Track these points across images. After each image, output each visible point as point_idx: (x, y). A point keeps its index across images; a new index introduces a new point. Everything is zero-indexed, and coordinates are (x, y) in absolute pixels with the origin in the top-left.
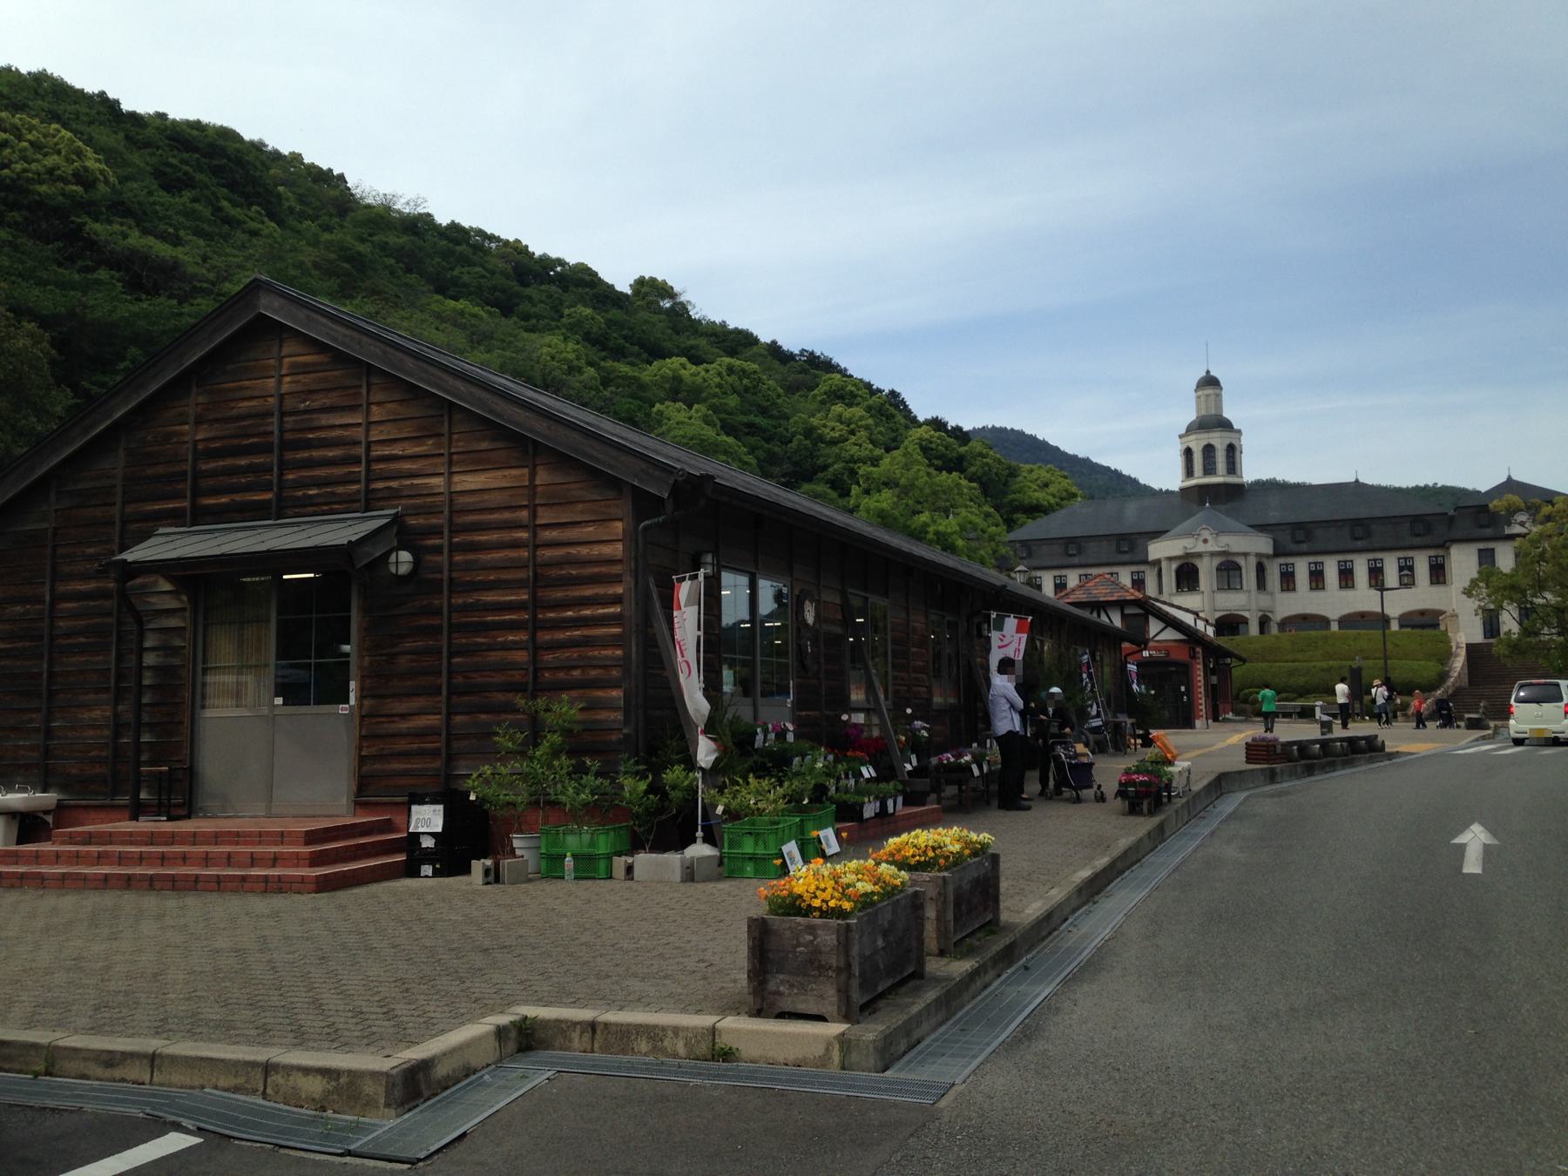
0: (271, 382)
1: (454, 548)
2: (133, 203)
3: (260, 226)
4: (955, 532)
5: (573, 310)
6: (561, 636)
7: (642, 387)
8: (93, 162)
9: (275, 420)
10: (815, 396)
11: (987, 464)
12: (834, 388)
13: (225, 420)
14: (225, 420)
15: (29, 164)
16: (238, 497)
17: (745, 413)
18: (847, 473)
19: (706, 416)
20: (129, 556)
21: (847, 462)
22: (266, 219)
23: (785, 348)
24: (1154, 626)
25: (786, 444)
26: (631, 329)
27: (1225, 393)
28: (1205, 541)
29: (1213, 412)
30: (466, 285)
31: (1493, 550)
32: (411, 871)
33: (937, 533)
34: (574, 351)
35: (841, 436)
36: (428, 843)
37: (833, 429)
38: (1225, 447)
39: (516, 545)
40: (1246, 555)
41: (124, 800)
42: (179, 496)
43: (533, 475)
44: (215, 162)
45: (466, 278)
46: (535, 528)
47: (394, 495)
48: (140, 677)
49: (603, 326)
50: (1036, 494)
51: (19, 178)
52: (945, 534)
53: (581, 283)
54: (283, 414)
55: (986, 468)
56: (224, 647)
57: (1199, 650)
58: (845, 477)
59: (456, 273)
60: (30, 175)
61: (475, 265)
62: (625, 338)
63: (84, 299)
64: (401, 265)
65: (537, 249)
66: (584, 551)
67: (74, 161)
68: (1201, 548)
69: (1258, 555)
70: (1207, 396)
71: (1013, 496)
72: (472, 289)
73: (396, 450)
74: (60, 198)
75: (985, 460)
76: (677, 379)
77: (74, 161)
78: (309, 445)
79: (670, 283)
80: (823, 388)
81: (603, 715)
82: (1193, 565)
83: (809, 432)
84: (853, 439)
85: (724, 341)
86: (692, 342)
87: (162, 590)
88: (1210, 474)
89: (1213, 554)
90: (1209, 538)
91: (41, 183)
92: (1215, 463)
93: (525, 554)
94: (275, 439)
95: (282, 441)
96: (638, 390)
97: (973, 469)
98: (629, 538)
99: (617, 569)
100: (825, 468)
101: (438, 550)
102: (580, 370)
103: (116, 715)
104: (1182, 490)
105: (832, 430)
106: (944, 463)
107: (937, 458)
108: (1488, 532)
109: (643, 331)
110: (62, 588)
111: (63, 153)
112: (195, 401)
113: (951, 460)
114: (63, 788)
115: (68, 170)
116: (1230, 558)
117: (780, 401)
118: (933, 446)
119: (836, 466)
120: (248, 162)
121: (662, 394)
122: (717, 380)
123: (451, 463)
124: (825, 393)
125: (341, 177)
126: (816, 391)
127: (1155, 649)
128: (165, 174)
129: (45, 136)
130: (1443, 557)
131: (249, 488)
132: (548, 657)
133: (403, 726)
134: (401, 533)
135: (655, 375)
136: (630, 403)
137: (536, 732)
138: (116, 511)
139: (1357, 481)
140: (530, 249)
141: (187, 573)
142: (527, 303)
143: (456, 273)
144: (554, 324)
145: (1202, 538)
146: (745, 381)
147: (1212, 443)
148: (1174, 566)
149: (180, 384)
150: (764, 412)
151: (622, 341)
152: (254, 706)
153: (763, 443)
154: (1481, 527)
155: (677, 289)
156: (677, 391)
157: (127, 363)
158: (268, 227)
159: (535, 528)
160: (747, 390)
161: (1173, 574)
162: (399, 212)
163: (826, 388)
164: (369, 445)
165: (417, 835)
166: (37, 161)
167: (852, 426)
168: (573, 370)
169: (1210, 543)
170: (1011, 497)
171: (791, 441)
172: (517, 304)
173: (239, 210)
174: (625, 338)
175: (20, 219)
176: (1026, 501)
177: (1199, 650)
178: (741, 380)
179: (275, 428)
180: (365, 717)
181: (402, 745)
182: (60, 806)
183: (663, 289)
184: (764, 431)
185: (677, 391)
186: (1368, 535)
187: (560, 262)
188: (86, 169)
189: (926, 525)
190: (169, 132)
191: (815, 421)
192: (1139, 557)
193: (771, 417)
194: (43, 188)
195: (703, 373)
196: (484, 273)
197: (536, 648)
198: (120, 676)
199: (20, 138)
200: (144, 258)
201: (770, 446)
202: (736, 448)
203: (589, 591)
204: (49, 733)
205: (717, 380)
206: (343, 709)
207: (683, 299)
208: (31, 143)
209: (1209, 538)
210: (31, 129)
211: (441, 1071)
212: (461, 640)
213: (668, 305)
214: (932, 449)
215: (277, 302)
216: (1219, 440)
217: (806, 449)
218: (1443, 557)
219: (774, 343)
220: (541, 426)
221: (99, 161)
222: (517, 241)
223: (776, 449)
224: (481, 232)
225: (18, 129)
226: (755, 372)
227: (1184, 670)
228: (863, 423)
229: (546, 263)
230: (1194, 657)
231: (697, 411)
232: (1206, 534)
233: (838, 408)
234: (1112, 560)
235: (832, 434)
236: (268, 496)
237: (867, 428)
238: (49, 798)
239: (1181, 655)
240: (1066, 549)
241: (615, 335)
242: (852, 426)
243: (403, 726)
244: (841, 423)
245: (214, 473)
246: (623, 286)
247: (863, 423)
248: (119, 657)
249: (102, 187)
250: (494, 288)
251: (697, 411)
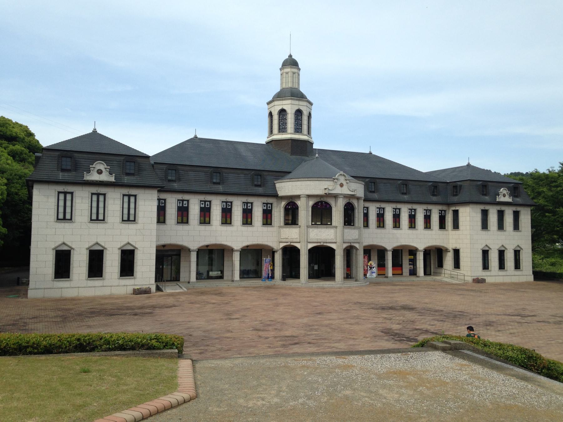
27: (301, 73)
28: (342, 185)
29: (290, 85)
38: (294, 111)
68: (338, 190)
69: (309, 196)
70: (287, 73)
88: (283, 132)
90: (344, 183)
104: (268, 143)
130: (445, 211)
139: (371, 153)
147: (284, 108)
148: (311, 203)
152: (268, 278)
161: (310, 209)
169: (345, 187)
176: (8, 133)
192: (270, 192)
209: (344, 183)
216: (290, 106)
218: (445, 211)
232: (342, 180)
234: (249, 191)
240: (212, 178)
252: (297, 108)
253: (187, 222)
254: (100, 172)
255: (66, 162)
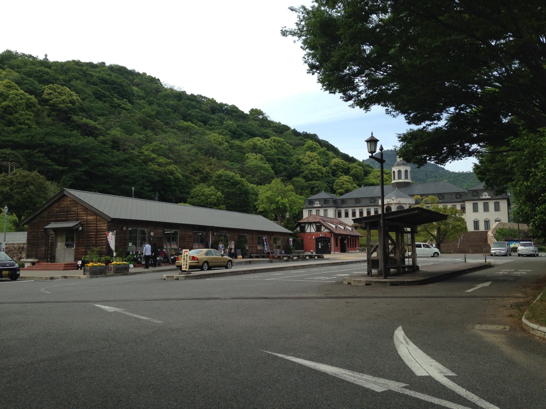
0: (66, 203)
1: (87, 227)
2: (85, 107)
3: (126, 106)
4: (287, 202)
5: (226, 122)
6: (99, 239)
7: (243, 148)
8: (75, 97)
9: (66, 208)
10: (303, 148)
11: (357, 170)
12: (309, 146)
13: (61, 208)
14: (61, 208)
15: (57, 99)
16: (62, 219)
17: (278, 155)
18: (309, 174)
19: (262, 157)
20: (46, 227)
21: (310, 170)
22: (128, 103)
23: (298, 131)
24: (323, 228)
25: (291, 164)
26: (245, 128)
28: (393, 200)
30: (193, 116)
31: (477, 203)
32: (78, 269)
33: (281, 203)
34: (222, 138)
35: (308, 162)
36: (80, 266)
37: (306, 160)
38: (404, 171)
39: (94, 226)
40: (406, 204)
41: (46, 261)
42: (53, 218)
43: (97, 217)
44: (114, 86)
45: (193, 113)
46: (97, 224)
47: (80, 219)
48: (48, 243)
49: (236, 127)
50: (373, 180)
51: (55, 103)
52: (284, 203)
53: (233, 111)
54: (67, 207)
55: (356, 172)
56: (59, 239)
57: (333, 234)
58: (309, 175)
59: (190, 112)
60: (58, 102)
61: (197, 108)
62: (243, 131)
63: (69, 140)
64: (173, 110)
65: (219, 101)
66: (102, 228)
67: (69, 97)
68: (392, 202)
69: (409, 204)
71: (366, 181)
72: (195, 117)
73: (81, 213)
74: (66, 108)
75: (356, 169)
76: (255, 145)
77: (69, 97)
78: (70, 212)
79: (262, 110)
80: (306, 145)
81: (103, 250)
82: (390, 207)
83: (298, 161)
84: (312, 163)
85: (279, 129)
86: (266, 131)
87: (52, 232)
88: (400, 179)
89: (395, 204)
90: (394, 199)
91: (61, 104)
92: (401, 176)
93: (95, 228)
94: (66, 211)
95: (67, 211)
96: (241, 150)
97: (352, 172)
98: (107, 226)
99: (106, 230)
100: (303, 172)
101: (85, 227)
102: (223, 144)
103: (45, 249)
105: (306, 160)
106: (343, 170)
107: (340, 169)
108: (476, 198)
109: (249, 128)
110: (39, 230)
111: (67, 95)
112: (57, 204)
113: (345, 169)
114: (38, 259)
115: (68, 100)
116: (401, 205)
117: (290, 151)
118: (339, 165)
119: (306, 172)
120: (124, 85)
121: (249, 150)
122: (270, 144)
123: (87, 215)
124: (307, 147)
125: (158, 80)
126: (304, 147)
127: (323, 234)
128: (97, 93)
129: (62, 90)
131: (62, 217)
132: (97, 242)
133: (80, 251)
134: (81, 224)
135: (247, 144)
136: (237, 154)
137: (93, 251)
138: (46, 219)
140: (217, 101)
141: (55, 230)
142: (212, 120)
143: (190, 112)
144: (219, 127)
145: (392, 199)
146: (279, 144)
149: (55, 202)
150: (284, 154)
151: (241, 132)
153: (283, 164)
154: (474, 196)
155: (264, 112)
156: (255, 149)
157: (63, 179)
158: (128, 106)
159: (97, 224)
160: (279, 147)
162: (176, 90)
163: (307, 146)
164: (77, 212)
165: (78, 265)
166: (60, 98)
167: (313, 159)
168: (220, 144)
170: (365, 181)
171: (292, 164)
172: (209, 121)
173: (119, 101)
174: (243, 131)
175: (55, 114)
177: (333, 234)
178: (278, 144)
179: (66, 209)
180: (76, 249)
181: (80, 253)
182: (38, 261)
183: (259, 112)
184: (284, 160)
185: (255, 149)
186: (443, 198)
187: (226, 105)
188: (73, 99)
189: (279, 200)
190: (100, 78)
191: (301, 157)
193: (287, 156)
194: (61, 106)
195: (265, 142)
196: (199, 111)
197: (96, 241)
198: (46, 243)
199: (55, 91)
200: (86, 125)
201: (285, 165)
202: (268, 168)
203: (102, 233)
204: (37, 251)
205: (270, 144)
206: (73, 248)
207: (266, 115)
208: (58, 93)
209: (394, 199)
210: (58, 88)
211: (55, 278)
212: (87, 239)
213: (261, 117)
214: (339, 166)
215: (66, 192)
217: (298, 166)
219: (294, 129)
220: (96, 211)
221: (76, 96)
222: (213, 99)
223: (287, 166)
224: (201, 96)
225: (55, 89)
226: (282, 141)
227: (329, 240)
228: (316, 157)
229: (222, 105)
230: (331, 236)
231: (259, 156)
232: (393, 198)
233: (308, 153)
234: (369, 205)
235: (306, 161)
236: (65, 219)
237: (317, 159)
238: (37, 260)
239: (328, 236)
241: (239, 130)
242: (313, 159)
243: (80, 251)
244: (309, 158)
245: (58, 215)
246: (247, 111)
247: (316, 157)
248: (46, 240)
249: (77, 104)
250: (202, 116)
251: (259, 156)
252: (405, 169)
253: (341, 217)
254: (485, 195)
255: (475, 194)
